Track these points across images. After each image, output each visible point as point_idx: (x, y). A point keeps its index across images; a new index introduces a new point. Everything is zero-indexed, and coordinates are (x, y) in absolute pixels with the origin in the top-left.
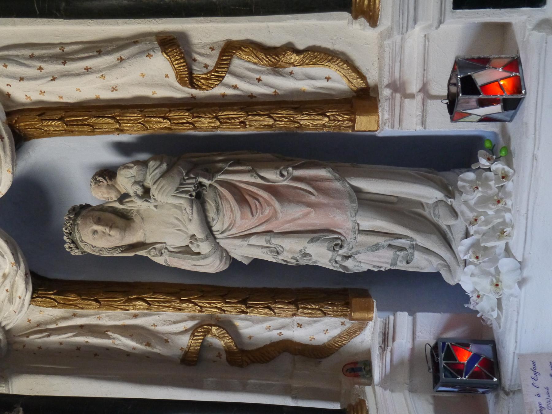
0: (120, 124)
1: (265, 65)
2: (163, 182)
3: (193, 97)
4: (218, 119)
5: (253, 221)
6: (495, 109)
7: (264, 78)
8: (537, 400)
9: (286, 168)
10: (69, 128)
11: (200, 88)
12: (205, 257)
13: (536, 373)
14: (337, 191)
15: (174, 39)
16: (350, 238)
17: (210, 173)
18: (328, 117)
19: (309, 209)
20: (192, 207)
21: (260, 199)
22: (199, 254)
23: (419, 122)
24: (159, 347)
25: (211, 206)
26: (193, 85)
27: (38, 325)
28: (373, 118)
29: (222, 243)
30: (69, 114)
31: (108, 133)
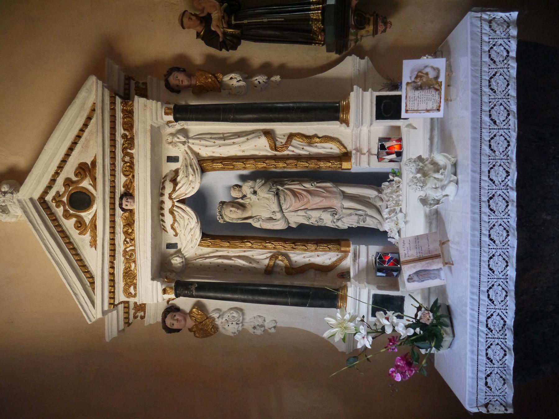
0: (245, 165)
1: (305, 142)
2: (263, 187)
3: (275, 155)
4: (286, 163)
5: (299, 204)
6: (393, 156)
7: (305, 148)
8: (404, 252)
9: (313, 183)
10: (224, 167)
11: (278, 151)
12: (279, 220)
13: (404, 244)
14: (334, 192)
15: (269, 132)
16: (339, 211)
17: (282, 185)
18: (331, 163)
19: (322, 199)
20: (275, 197)
21: (303, 195)
22: (276, 219)
23: (367, 163)
24: (255, 264)
25: (282, 198)
26: (276, 150)
27: (200, 256)
28: (349, 163)
29: (286, 214)
30: (224, 161)
31: (240, 169)
